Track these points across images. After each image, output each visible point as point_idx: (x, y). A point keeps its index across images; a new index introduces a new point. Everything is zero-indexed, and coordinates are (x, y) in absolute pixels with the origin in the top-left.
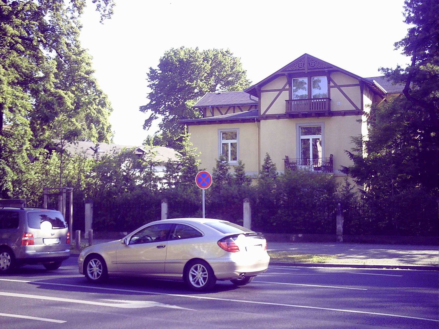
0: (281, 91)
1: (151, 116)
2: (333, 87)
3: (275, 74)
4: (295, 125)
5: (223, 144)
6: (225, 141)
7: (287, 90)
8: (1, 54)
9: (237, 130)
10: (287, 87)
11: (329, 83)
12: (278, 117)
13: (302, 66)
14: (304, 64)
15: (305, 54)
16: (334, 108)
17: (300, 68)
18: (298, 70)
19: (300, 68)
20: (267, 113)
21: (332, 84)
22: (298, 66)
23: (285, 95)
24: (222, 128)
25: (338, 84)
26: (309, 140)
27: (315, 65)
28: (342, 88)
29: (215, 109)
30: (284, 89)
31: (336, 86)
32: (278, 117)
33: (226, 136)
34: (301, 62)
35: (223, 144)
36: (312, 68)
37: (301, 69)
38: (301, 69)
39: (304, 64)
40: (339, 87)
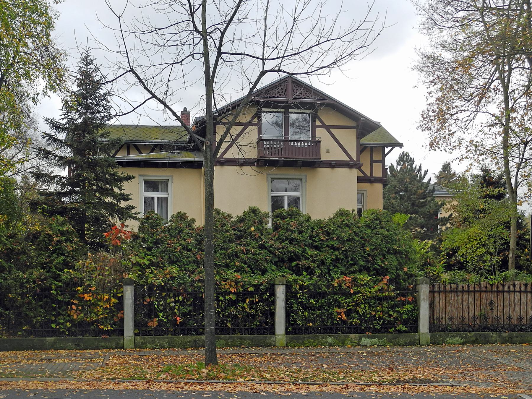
0: (246, 125)
2: (319, 127)
4: (265, 176)
5: (363, 193)
6: (150, 194)
7: (255, 125)
8: (1, 371)
9: (170, 178)
13: (283, 93)
14: (286, 90)
16: (324, 157)
18: (278, 97)
19: (280, 95)
24: (147, 174)
25: (327, 124)
26: (153, 198)
27: (301, 93)
29: (132, 147)
31: (323, 126)
33: (151, 185)
35: (363, 193)
36: (298, 97)
37: (281, 96)
38: (281, 96)
40: (328, 128)
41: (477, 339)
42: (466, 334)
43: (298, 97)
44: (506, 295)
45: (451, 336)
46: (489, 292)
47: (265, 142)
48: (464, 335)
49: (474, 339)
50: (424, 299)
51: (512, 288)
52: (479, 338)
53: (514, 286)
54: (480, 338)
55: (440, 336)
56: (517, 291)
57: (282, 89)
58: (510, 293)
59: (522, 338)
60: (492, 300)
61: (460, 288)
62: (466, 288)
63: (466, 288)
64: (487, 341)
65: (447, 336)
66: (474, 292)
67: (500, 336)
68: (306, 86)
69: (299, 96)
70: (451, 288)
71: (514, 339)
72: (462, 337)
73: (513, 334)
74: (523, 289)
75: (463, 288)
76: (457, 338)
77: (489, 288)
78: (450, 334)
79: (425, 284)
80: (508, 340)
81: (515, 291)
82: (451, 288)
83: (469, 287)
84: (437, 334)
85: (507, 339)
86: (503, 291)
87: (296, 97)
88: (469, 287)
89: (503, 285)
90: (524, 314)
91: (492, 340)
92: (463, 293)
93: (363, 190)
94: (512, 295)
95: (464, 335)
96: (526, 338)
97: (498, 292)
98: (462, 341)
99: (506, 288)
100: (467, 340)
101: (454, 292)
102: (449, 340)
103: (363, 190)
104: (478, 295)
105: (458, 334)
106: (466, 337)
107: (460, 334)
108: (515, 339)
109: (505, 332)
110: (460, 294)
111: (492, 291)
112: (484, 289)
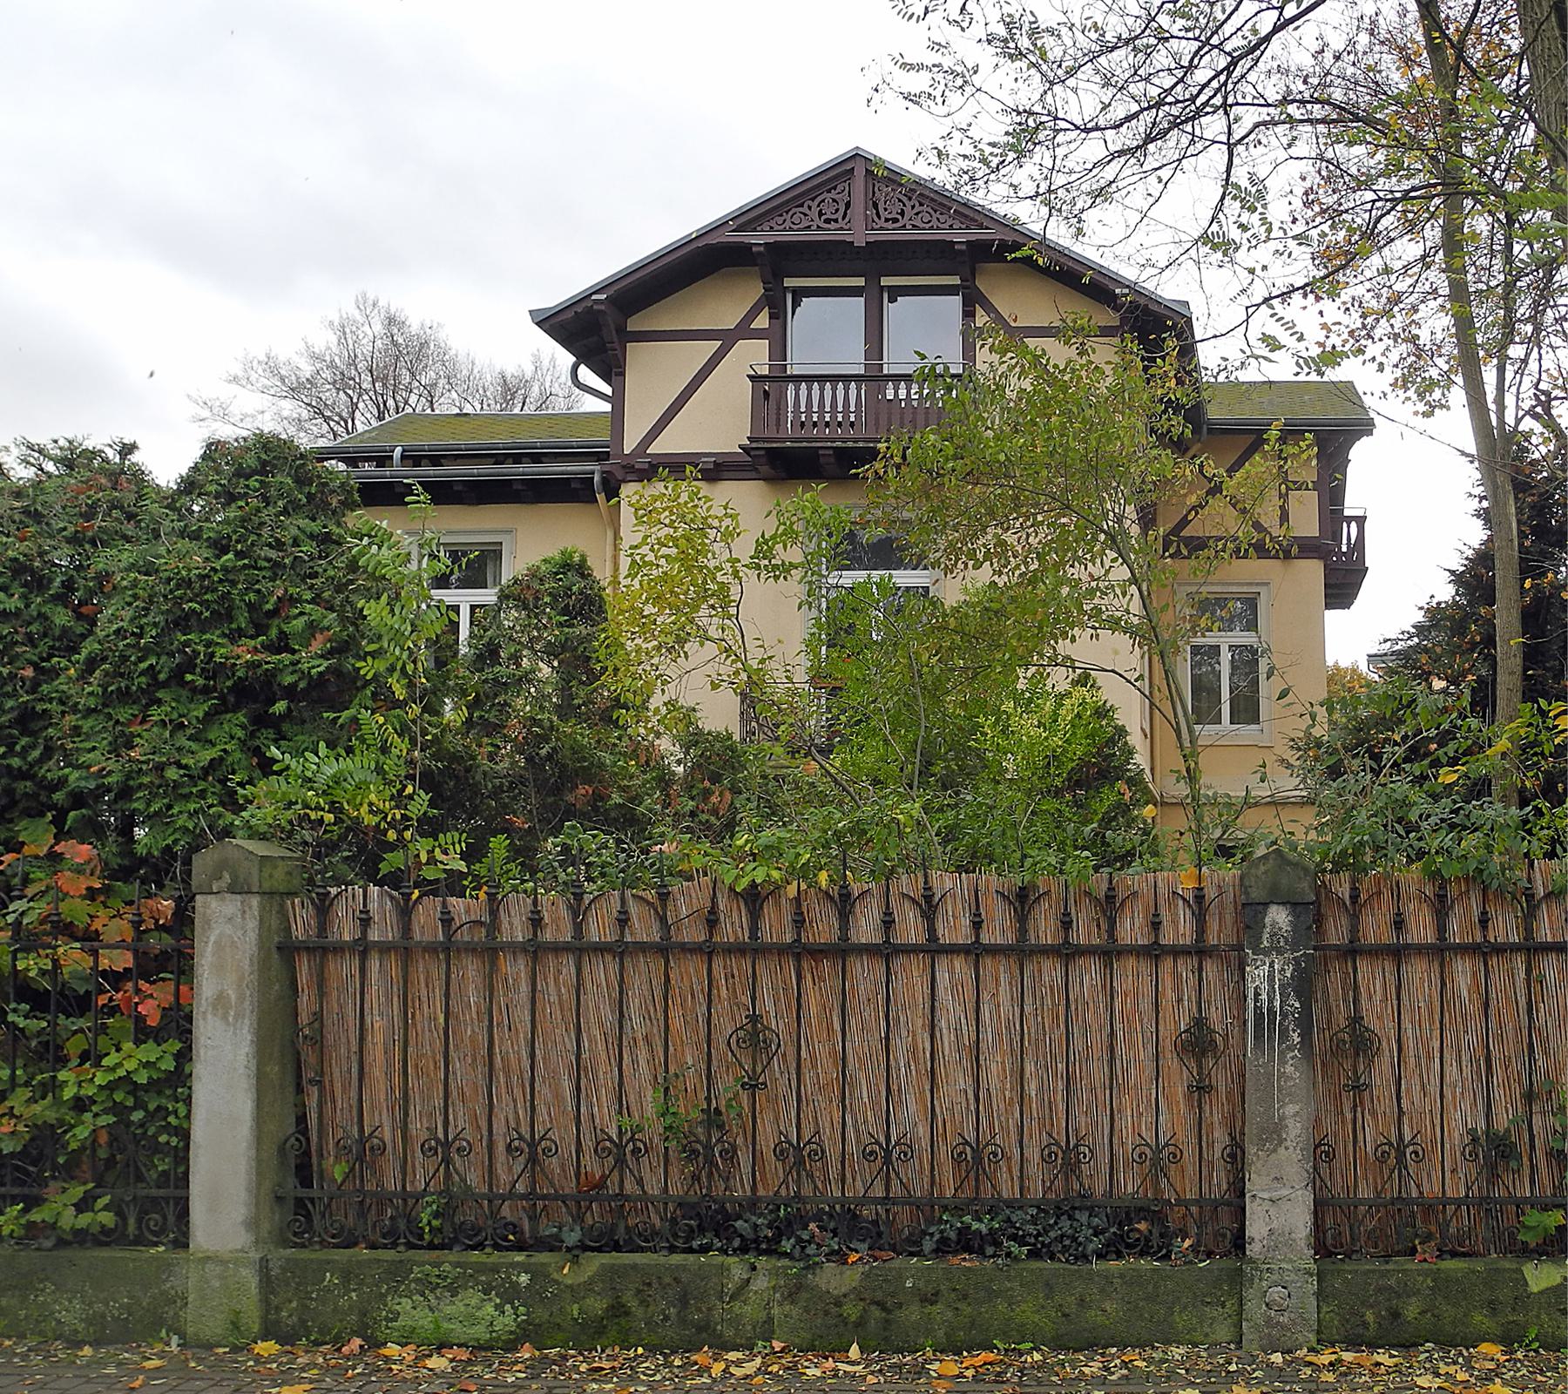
0: (728, 339)
1: (1181, 747)
3: (713, 240)
7: (759, 334)
10: (762, 321)
11: (969, 314)
12: (717, 470)
13: (839, 215)
14: (848, 205)
15: (856, 156)
17: (828, 221)
19: (828, 221)
20: (667, 444)
21: (981, 319)
22: (821, 214)
23: (753, 355)
26: (1216, 649)
27: (902, 213)
28: (1188, 154)
30: (744, 331)
32: (717, 470)
34: (833, 194)
38: (833, 225)
39: (848, 205)
41: (618, 1310)
42: (537, 1273)
43: (890, 225)
44: (865, 974)
45: (427, 1285)
46: (1046, 951)
47: (791, 386)
48: (524, 1279)
49: (597, 1305)
50: (220, 1000)
51: (910, 929)
52: (633, 1304)
53: (929, 907)
54: (644, 1303)
55: (347, 1275)
56: (953, 950)
57: (834, 200)
58: (851, 959)
59: (967, 1310)
60: (754, 1019)
61: (515, 928)
62: (558, 929)
63: (558, 929)
64: (700, 1329)
65: (397, 1275)
66: (975, 951)
67: (799, 1287)
68: (962, 209)
69: (895, 220)
70: (447, 920)
71: (901, 1315)
72: (510, 1294)
73: (901, 1278)
74: (999, 930)
75: (536, 922)
76: (472, 1297)
77: (734, 926)
78: (423, 1263)
79: (232, 890)
80: (861, 1323)
81: (933, 949)
82: (447, 920)
83: (578, 912)
84: (327, 1264)
85: (852, 1311)
86: (842, 951)
87: (885, 225)
88: (578, 912)
89: (844, 904)
90: (1004, 1120)
91: (736, 1321)
92: (494, 963)
93: (1257, 584)
94: (427, 971)
95: (524, 1279)
96: (1002, 1306)
97: (801, 952)
98: (507, 1322)
99: (866, 929)
100: (541, 1314)
101: (471, 949)
102: (411, 1311)
103: (1257, 584)
104: (643, 976)
105: (481, 1268)
106: (532, 1296)
107: (495, 1269)
108: (912, 1313)
109: (839, 1257)
110: (515, 969)
111: (753, 949)
112: (693, 933)
